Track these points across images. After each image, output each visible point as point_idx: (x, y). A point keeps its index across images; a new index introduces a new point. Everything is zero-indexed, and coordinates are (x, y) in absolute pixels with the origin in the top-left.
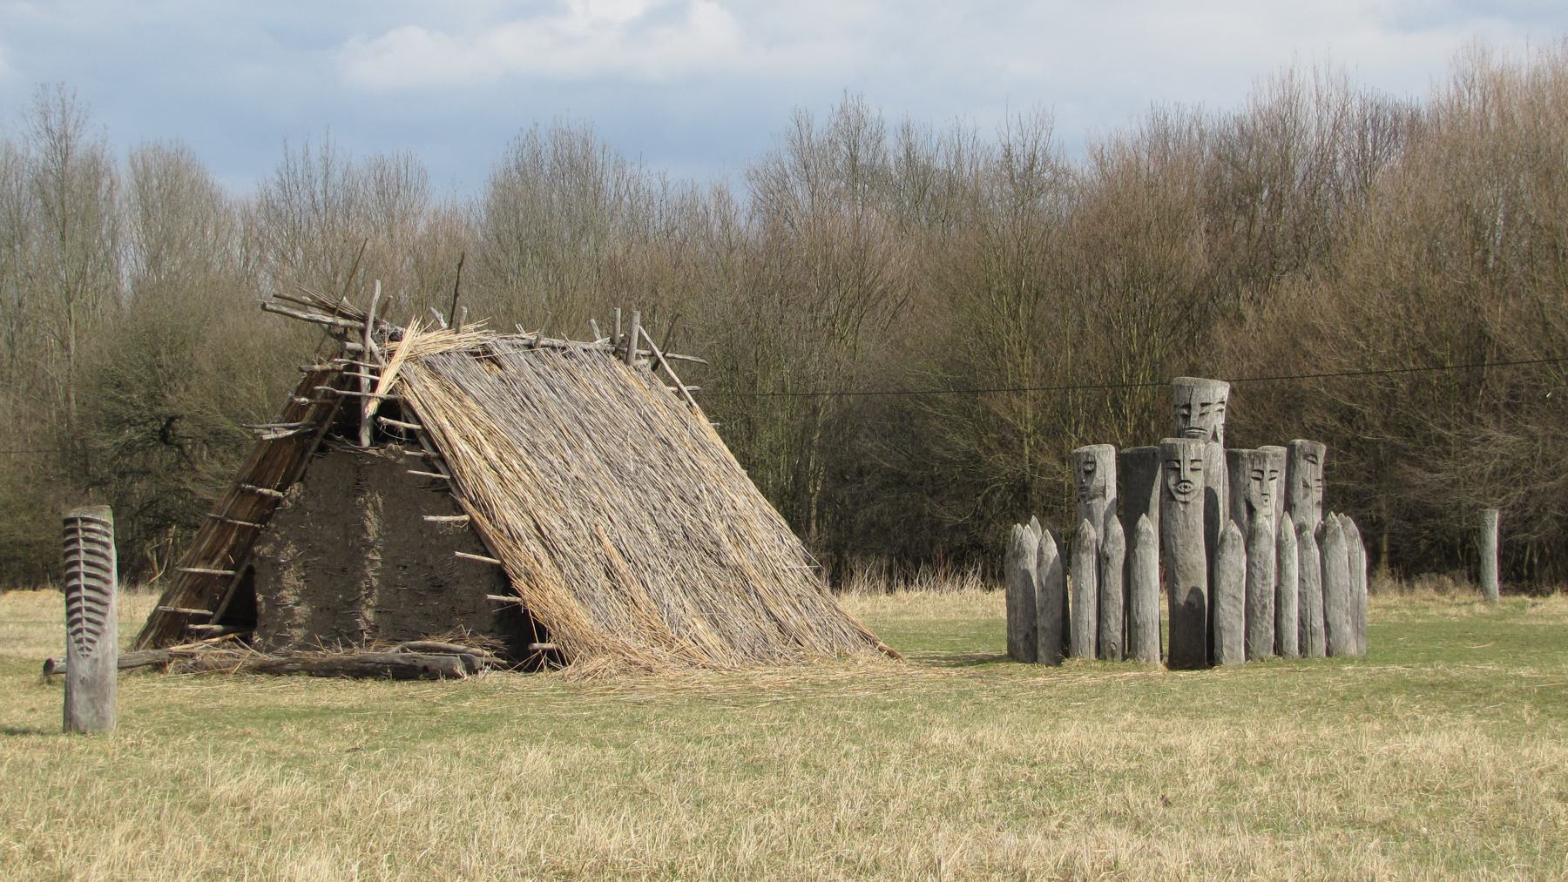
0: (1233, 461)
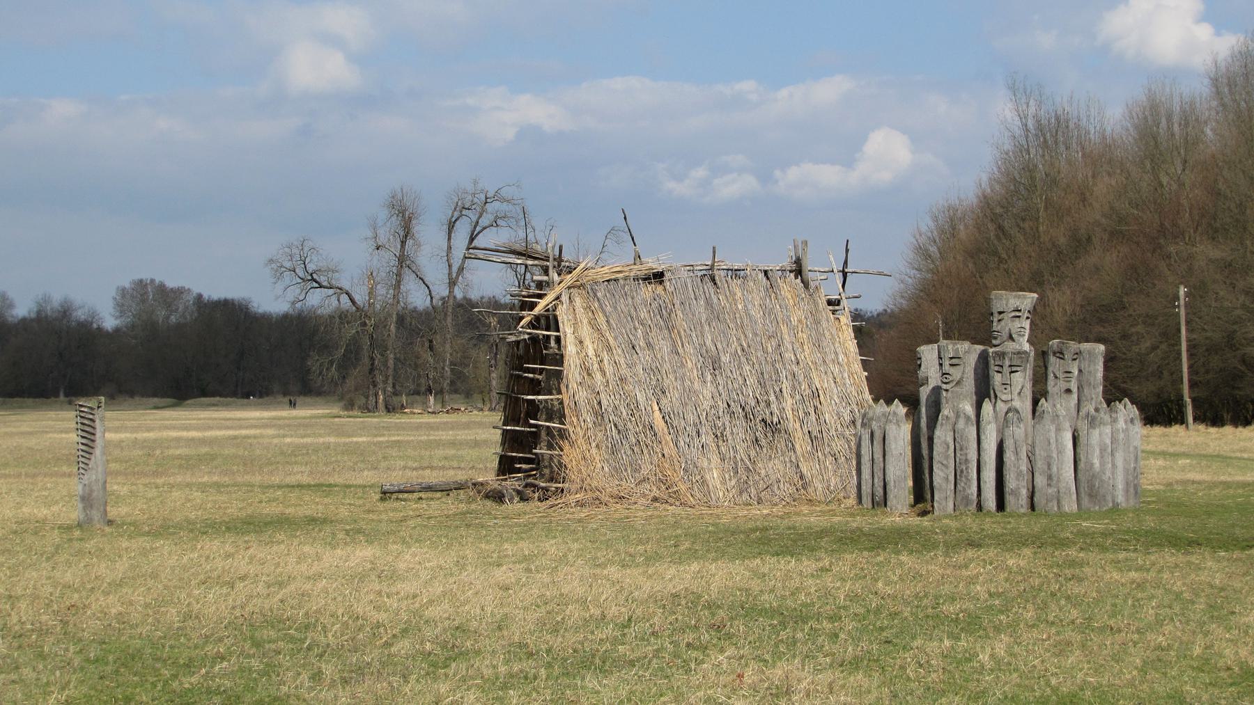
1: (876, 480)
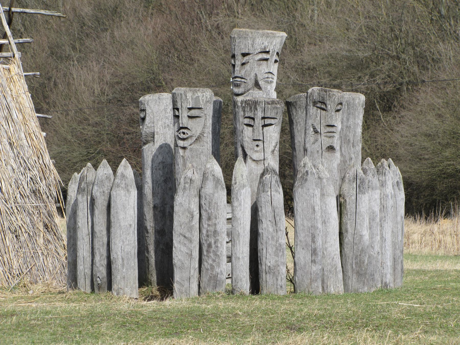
1: (97, 258)
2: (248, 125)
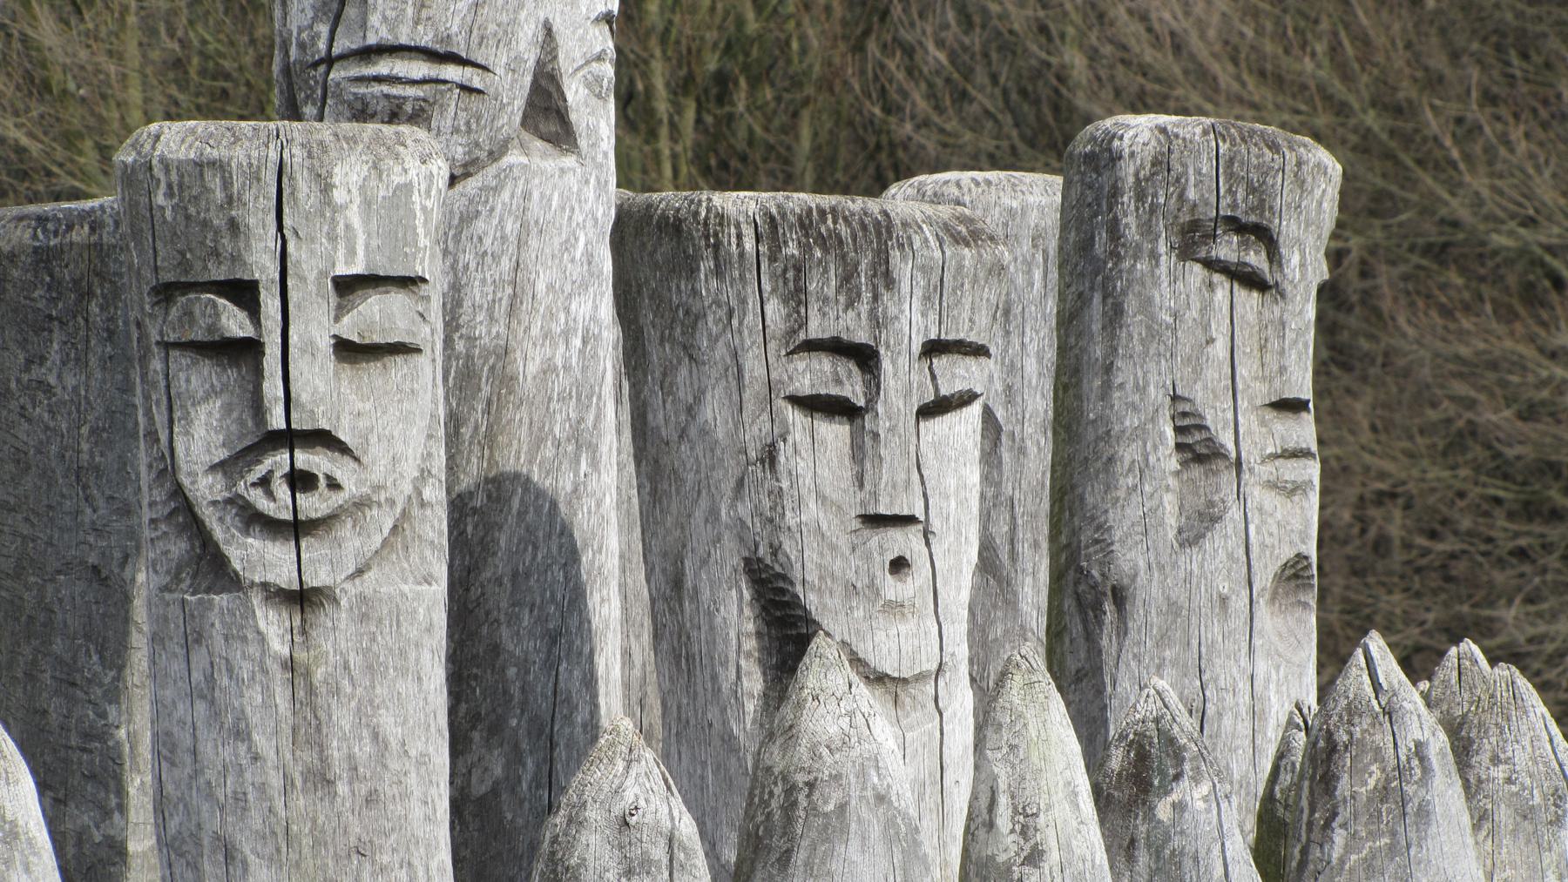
0: (654, 265)
2: (815, 405)
